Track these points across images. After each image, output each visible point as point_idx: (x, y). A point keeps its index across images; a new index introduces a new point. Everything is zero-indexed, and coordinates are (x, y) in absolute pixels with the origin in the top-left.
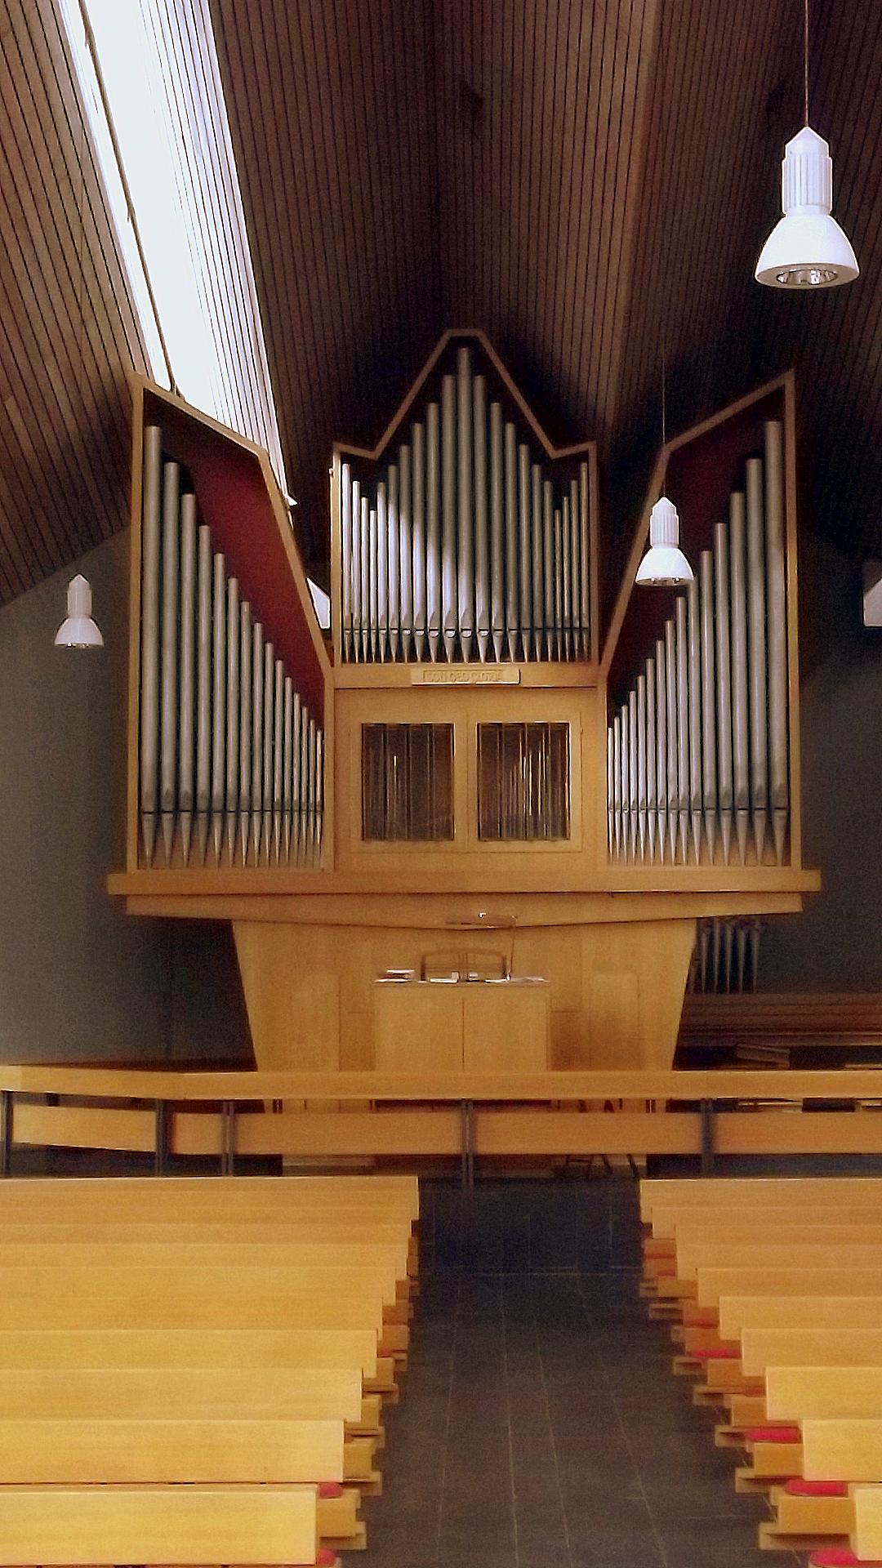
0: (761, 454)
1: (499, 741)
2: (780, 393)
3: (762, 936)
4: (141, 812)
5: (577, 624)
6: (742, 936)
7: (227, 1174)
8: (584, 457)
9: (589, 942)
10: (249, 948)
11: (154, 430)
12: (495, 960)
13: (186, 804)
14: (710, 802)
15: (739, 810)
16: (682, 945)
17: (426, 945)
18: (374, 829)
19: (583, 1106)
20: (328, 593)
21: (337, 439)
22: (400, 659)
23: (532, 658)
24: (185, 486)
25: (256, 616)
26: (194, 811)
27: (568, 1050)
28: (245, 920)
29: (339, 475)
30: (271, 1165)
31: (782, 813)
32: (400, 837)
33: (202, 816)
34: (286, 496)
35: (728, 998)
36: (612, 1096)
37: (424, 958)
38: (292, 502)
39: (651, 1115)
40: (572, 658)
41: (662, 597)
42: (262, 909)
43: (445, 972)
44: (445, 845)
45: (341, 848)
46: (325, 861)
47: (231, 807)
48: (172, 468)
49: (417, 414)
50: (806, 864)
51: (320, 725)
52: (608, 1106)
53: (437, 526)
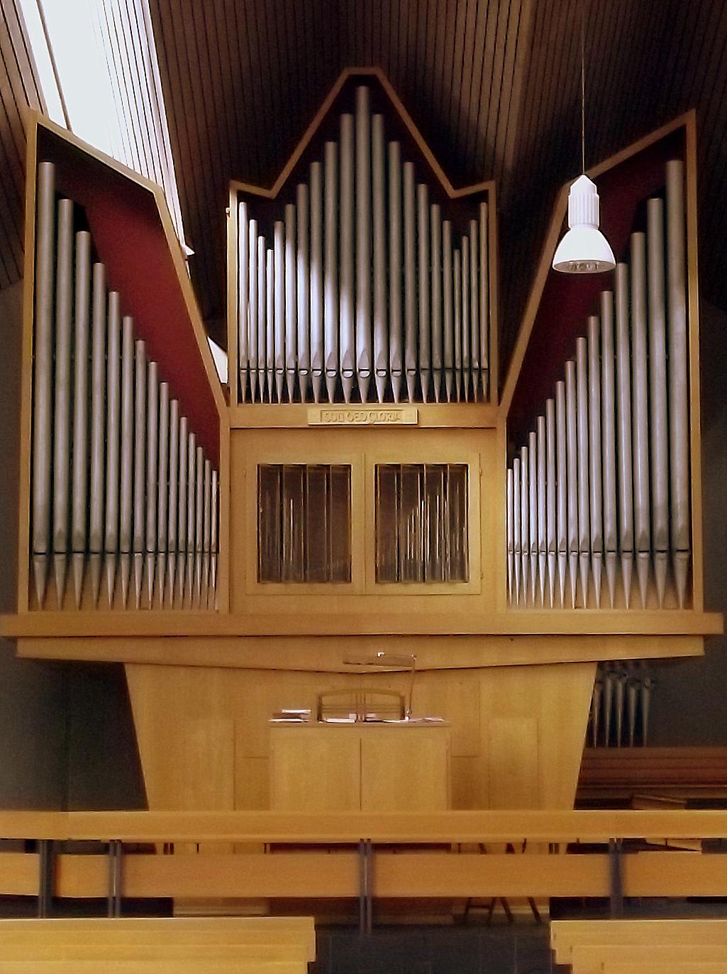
0: (662, 194)
1: (398, 484)
2: (682, 131)
3: (653, 692)
4: (32, 553)
5: (476, 365)
6: (633, 692)
7: (114, 916)
8: (483, 196)
9: (488, 686)
10: (143, 692)
11: (47, 167)
12: (394, 700)
13: (78, 545)
14: (611, 545)
15: (639, 552)
16: (578, 694)
17: (321, 686)
18: (268, 573)
19: (482, 848)
20: (224, 348)
21: (234, 178)
22: (297, 399)
23: (431, 399)
24: (79, 222)
25: (151, 355)
26: (87, 552)
27: (468, 788)
28: (135, 663)
29: (236, 212)
30: (163, 907)
31: (684, 556)
32: (297, 580)
33: (95, 559)
34: (183, 245)
35: (620, 751)
36: (516, 837)
37: (320, 698)
38: (189, 252)
39: (554, 856)
40: (471, 399)
41: (581, 291)
42: (153, 651)
43: (343, 712)
44: (341, 587)
45: (238, 589)
46: (220, 603)
47: (124, 549)
48: (66, 204)
49: (315, 152)
50: (708, 607)
51: (215, 467)
52: (510, 849)
53: (332, 261)
